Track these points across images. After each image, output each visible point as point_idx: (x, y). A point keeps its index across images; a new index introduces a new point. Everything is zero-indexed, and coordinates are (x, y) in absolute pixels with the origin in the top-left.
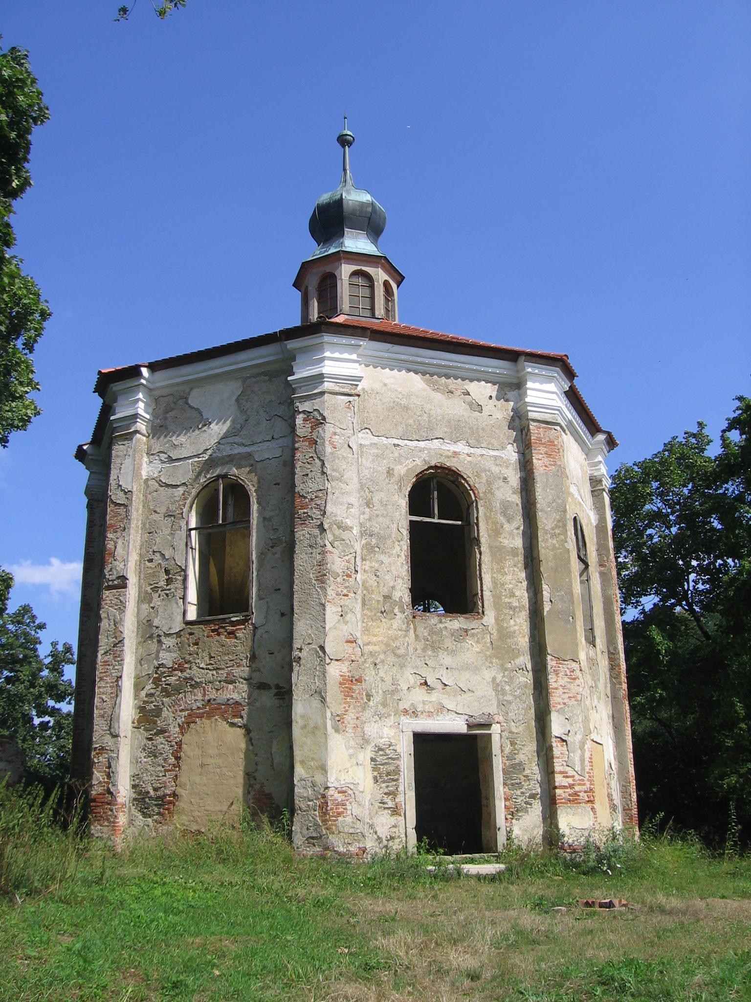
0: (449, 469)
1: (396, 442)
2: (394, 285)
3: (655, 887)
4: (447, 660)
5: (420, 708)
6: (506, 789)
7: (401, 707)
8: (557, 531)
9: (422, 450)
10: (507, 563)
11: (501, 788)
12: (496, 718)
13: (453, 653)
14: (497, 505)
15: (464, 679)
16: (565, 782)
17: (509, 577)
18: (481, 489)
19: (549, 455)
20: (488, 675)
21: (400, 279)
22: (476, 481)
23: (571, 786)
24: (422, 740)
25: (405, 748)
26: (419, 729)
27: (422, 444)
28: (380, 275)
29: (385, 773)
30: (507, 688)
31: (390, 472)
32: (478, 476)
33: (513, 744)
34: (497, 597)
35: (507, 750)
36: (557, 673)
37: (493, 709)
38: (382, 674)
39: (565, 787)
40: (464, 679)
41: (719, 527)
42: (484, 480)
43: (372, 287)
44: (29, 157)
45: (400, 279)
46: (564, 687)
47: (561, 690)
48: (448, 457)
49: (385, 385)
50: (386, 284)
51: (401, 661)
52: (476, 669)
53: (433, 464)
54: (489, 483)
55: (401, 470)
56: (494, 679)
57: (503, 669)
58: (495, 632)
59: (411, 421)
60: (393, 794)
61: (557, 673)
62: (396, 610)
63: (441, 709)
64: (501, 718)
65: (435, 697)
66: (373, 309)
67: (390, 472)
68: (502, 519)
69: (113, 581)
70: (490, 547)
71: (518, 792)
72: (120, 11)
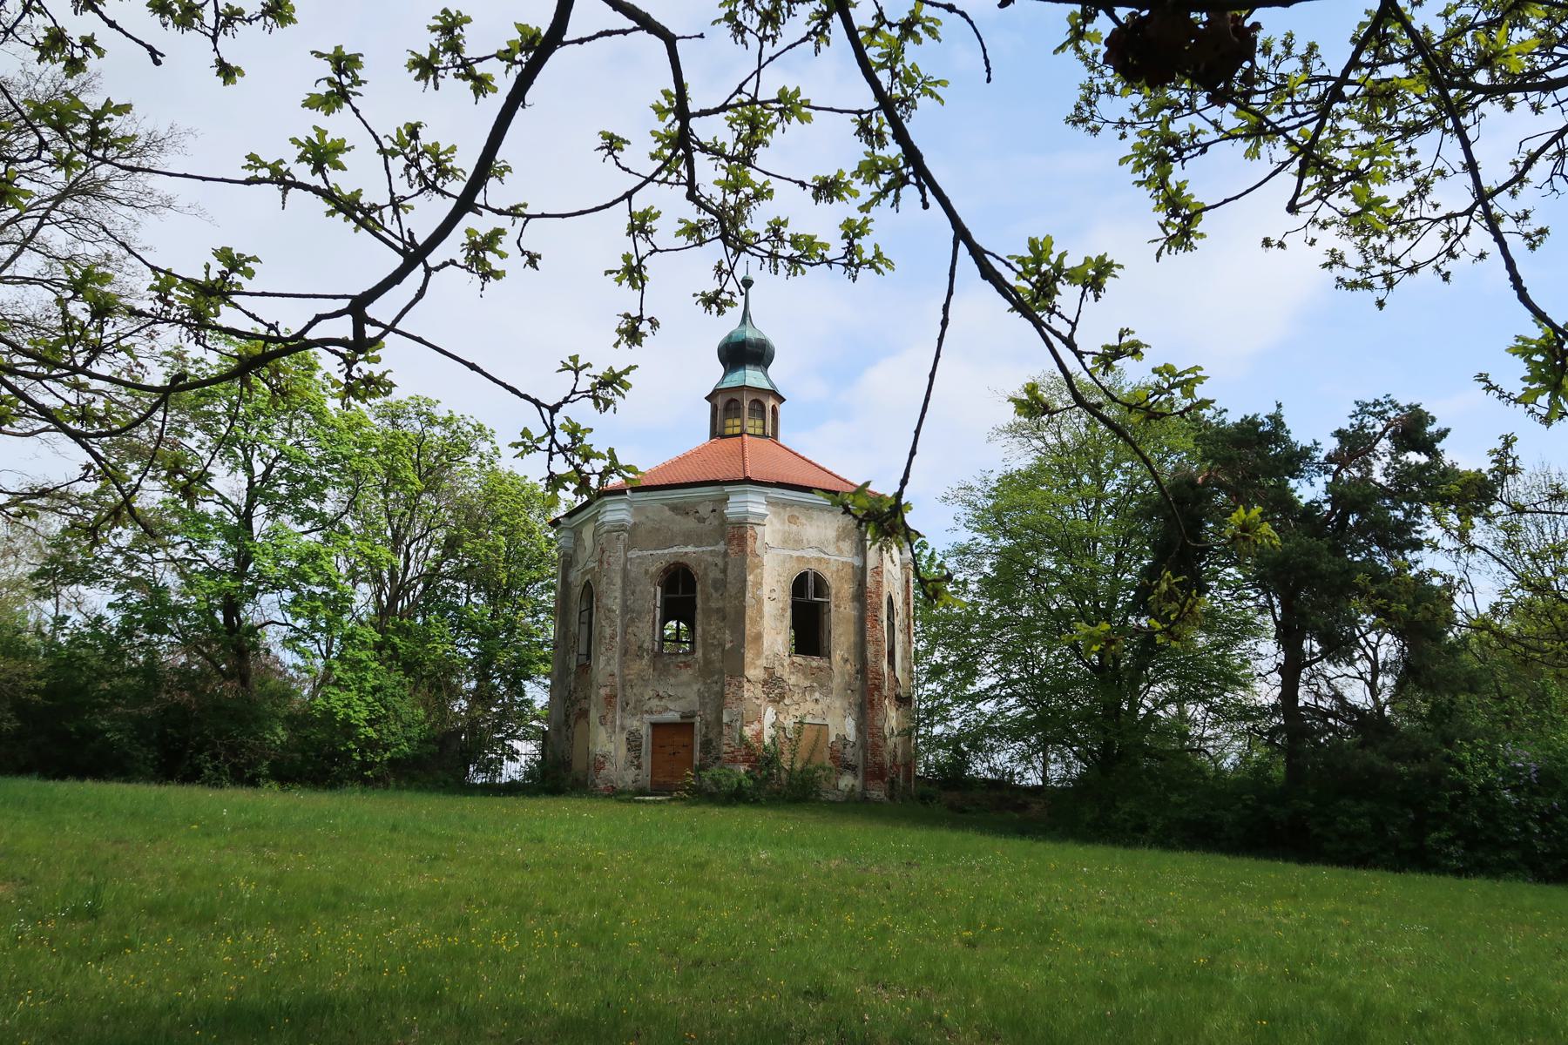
3: (612, 945)
4: (672, 680)
13: (675, 676)
15: (680, 691)
18: (700, 573)
20: (695, 688)
21: (781, 400)
22: (698, 571)
25: (645, 731)
29: (634, 744)
31: (646, 572)
34: (704, 640)
40: (680, 691)
41: (1193, 15)
44: (347, 192)
50: (774, 409)
51: (646, 682)
52: (688, 685)
55: (653, 569)
60: (638, 757)
63: (667, 709)
67: (646, 572)
69: (408, 547)
72: (488, 274)
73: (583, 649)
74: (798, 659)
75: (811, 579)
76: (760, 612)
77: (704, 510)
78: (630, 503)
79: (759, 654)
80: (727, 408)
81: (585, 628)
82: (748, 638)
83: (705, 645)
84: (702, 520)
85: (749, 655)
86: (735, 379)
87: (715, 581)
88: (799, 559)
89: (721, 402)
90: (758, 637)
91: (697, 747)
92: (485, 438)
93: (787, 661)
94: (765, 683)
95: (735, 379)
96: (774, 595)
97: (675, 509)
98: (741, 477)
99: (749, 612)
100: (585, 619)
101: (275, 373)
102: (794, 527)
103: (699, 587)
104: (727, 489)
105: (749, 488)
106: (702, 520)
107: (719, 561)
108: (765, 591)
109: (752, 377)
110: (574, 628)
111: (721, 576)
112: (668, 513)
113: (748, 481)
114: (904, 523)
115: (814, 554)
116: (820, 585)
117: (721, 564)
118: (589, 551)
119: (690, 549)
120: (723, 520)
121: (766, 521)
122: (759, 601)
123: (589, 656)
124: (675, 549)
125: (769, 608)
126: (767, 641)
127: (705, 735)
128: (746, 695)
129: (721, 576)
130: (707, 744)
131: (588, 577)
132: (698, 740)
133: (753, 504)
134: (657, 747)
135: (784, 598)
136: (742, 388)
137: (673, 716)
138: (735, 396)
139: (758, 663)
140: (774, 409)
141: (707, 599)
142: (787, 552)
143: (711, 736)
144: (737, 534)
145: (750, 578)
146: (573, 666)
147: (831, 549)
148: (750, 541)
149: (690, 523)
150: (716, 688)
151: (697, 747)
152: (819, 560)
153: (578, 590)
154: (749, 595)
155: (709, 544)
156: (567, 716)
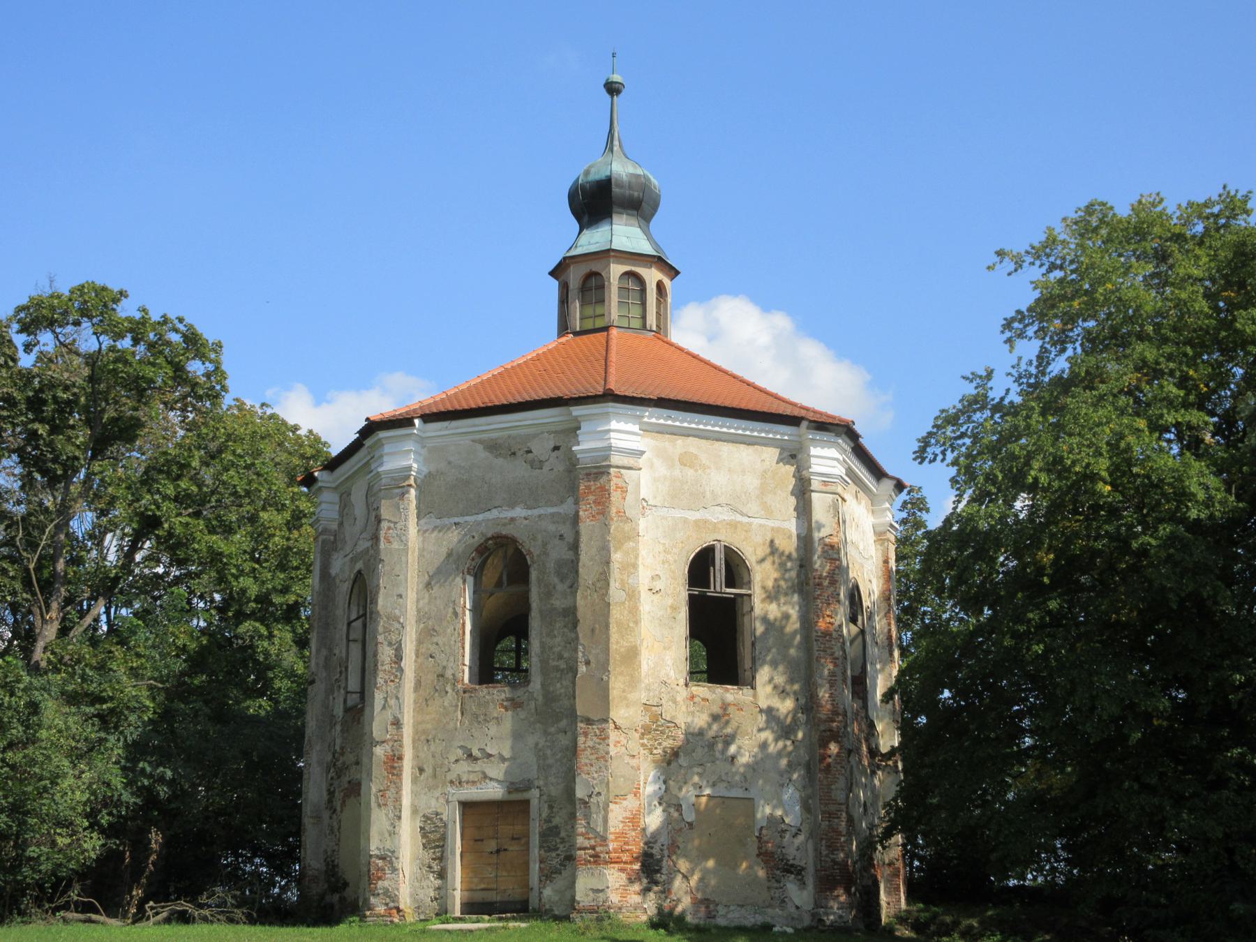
0: (506, 537)
1: (456, 520)
2: (666, 281)
5: (464, 778)
6: (542, 852)
7: (449, 778)
8: (598, 585)
9: (479, 524)
10: (558, 625)
11: (536, 851)
12: (536, 783)
14: (551, 565)
16: (587, 843)
17: (558, 639)
19: (596, 502)
21: (673, 272)
22: (532, 548)
23: (593, 848)
24: (467, 807)
26: (463, 798)
27: (480, 517)
28: (652, 276)
30: (549, 752)
32: (534, 539)
33: (551, 807)
35: (544, 815)
36: (586, 734)
37: (533, 774)
38: (432, 748)
39: (585, 849)
42: (539, 542)
43: (643, 290)
45: (673, 272)
46: (592, 748)
47: (589, 751)
48: (504, 525)
49: (450, 463)
50: (660, 287)
53: (489, 535)
54: (545, 544)
56: (537, 744)
57: (546, 733)
58: (540, 698)
59: (472, 496)
61: (586, 734)
62: (449, 688)
64: (541, 783)
65: (478, 767)
66: (644, 317)
68: (556, 580)
70: (541, 612)
71: (554, 854)
73: (353, 683)
74: (703, 690)
75: (719, 557)
76: (634, 611)
77: (541, 448)
78: (421, 440)
79: (634, 682)
80: (584, 289)
81: (355, 649)
82: (614, 656)
83: (545, 671)
84: (537, 464)
85: (616, 685)
86: (594, 239)
87: (560, 564)
88: (700, 525)
89: (575, 276)
90: (632, 655)
91: (535, 840)
92: (202, 357)
93: (682, 694)
94: (646, 731)
95: (594, 239)
96: (658, 585)
97: (493, 447)
98: (600, 390)
99: (616, 614)
100: (356, 634)
101: (222, 460)
102: (690, 472)
103: (534, 575)
104: (577, 411)
105: (611, 407)
106: (537, 464)
107: (566, 530)
108: (643, 578)
109: (623, 234)
110: (340, 651)
111: (569, 555)
112: (482, 454)
113: (609, 396)
114: (941, 529)
115: (723, 515)
116: (736, 569)
117: (569, 537)
118: (360, 523)
119: (519, 512)
120: (572, 462)
121: (642, 462)
122: (633, 595)
123: (362, 693)
124: (494, 514)
125: (648, 606)
126: (646, 661)
127: (548, 820)
128: (613, 751)
129: (569, 555)
130: (550, 834)
131: (359, 565)
132: (535, 828)
133: (622, 432)
134: (473, 843)
135: (678, 593)
136: (607, 254)
137: (493, 791)
138: (595, 266)
139: (633, 696)
140: (660, 287)
141: (548, 594)
142: (678, 514)
143: (556, 821)
144: (586, 480)
145: (616, 557)
146: (339, 711)
147: (753, 508)
148: (615, 496)
149: (518, 470)
150: (564, 741)
151: (535, 840)
152: (734, 525)
153: (345, 587)
154: (614, 585)
155: (550, 503)
156: (331, 793)
